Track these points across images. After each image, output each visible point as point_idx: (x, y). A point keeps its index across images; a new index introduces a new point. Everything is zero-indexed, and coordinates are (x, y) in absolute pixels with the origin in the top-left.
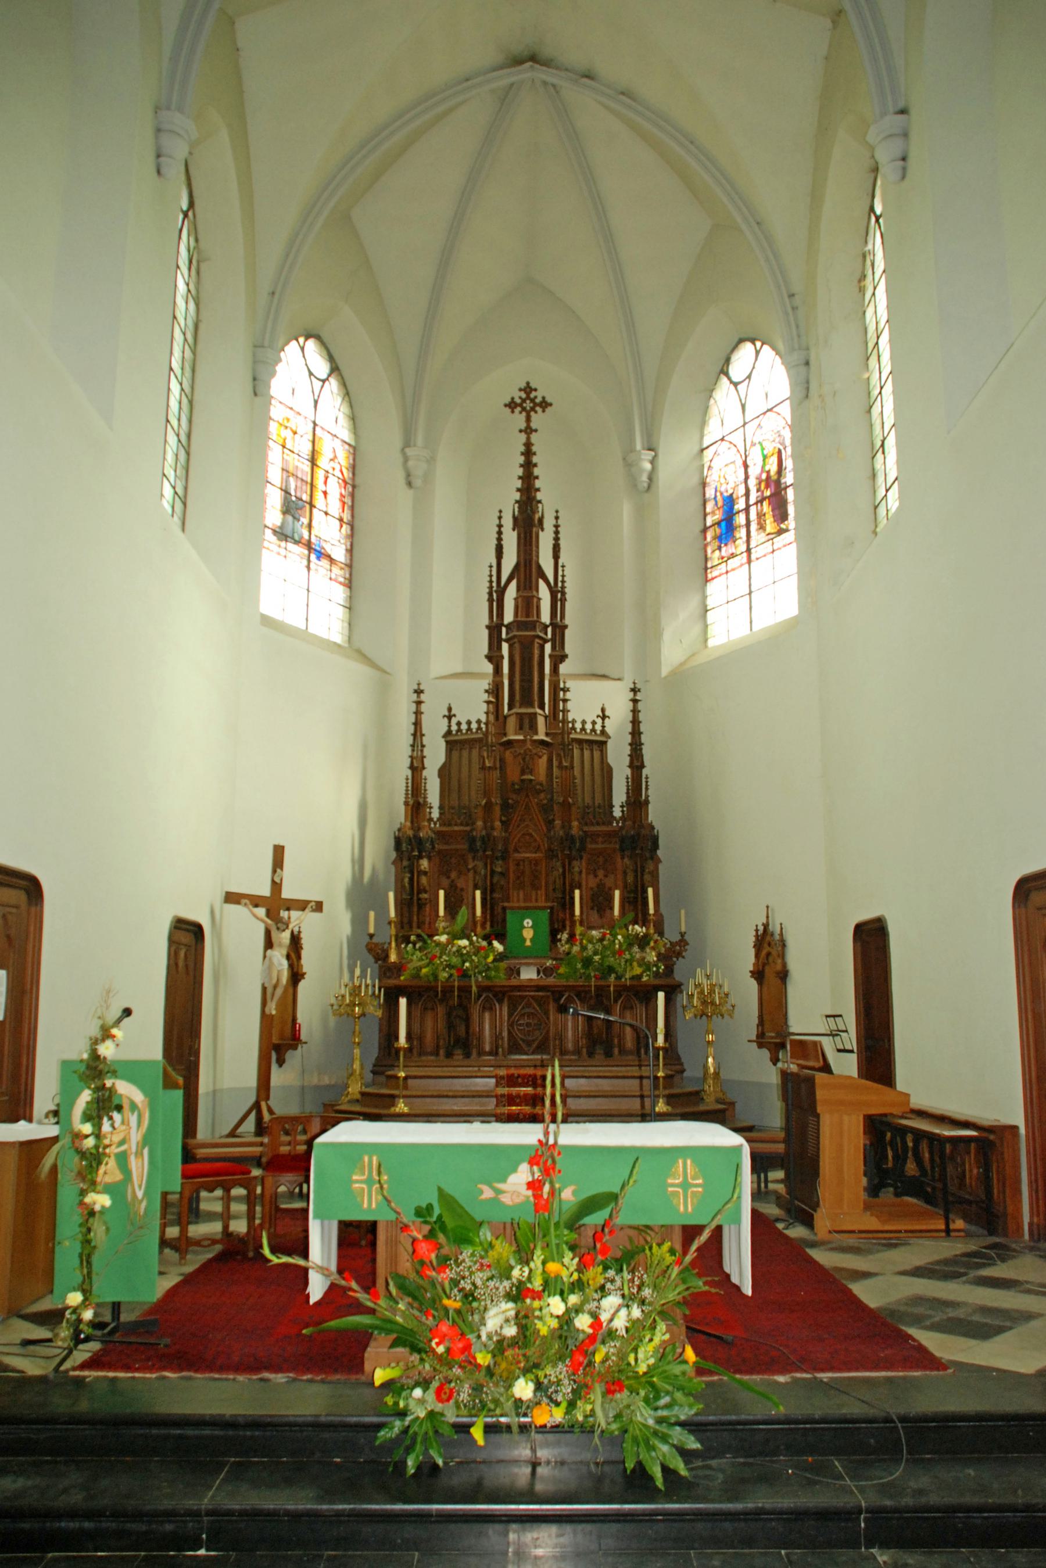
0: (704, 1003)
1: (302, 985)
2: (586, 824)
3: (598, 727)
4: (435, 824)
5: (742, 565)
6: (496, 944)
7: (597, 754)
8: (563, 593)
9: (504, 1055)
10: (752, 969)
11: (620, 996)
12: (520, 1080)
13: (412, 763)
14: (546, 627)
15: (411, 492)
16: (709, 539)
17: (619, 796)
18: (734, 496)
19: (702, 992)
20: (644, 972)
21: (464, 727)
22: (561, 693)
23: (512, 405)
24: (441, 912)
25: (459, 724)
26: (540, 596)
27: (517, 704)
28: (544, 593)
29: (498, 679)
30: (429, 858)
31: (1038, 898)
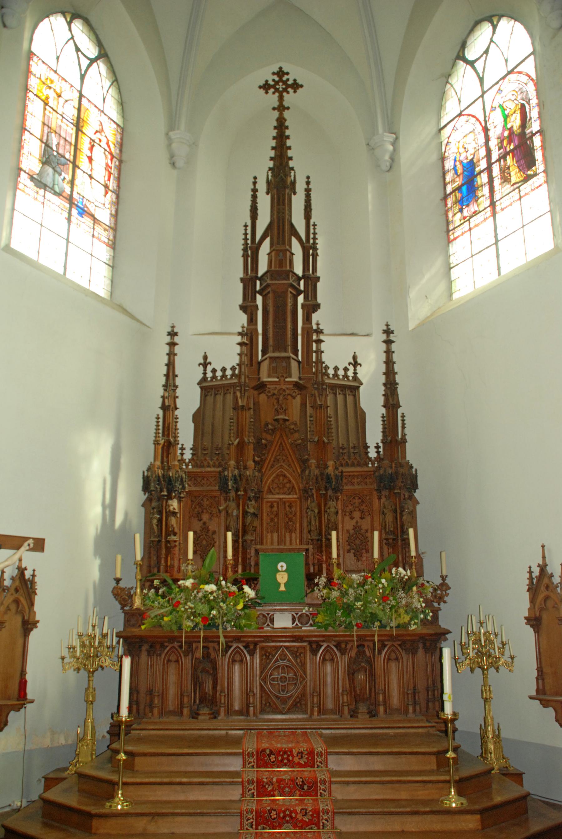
0: (480, 654)
1: (34, 636)
2: (342, 465)
3: (350, 373)
4: (187, 465)
5: (486, 219)
6: (246, 588)
7: (350, 399)
8: (315, 249)
9: (254, 714)
10: (527, 615)
11: (384, 646)
12: (273, 758)
13: (164, 402)
14: (299, 279)
15: (175, 172)
16: (449, 205)
17: (374, 435)
18: (475, 160)
19: (477, 641)
20: (412, 619)
21: (219, 374)
22: (314, 345)
23: (266, 87)
24: (190, 556)
25: (214, 371)
26: (293, 251)
27: (271, 349)
28: (296, 248)
29: (253, 327)
30: (180, 500)
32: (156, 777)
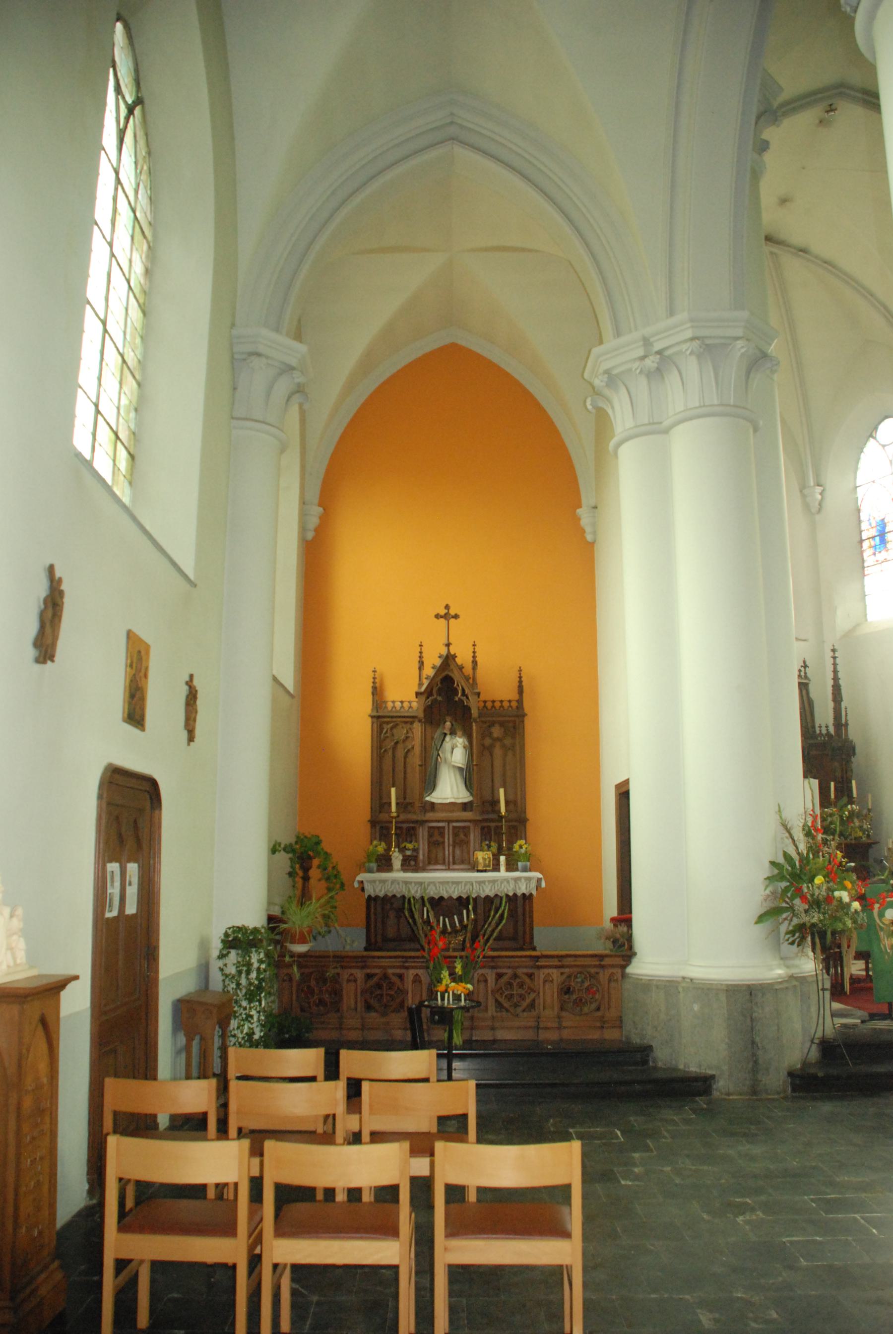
31: (146, 786)
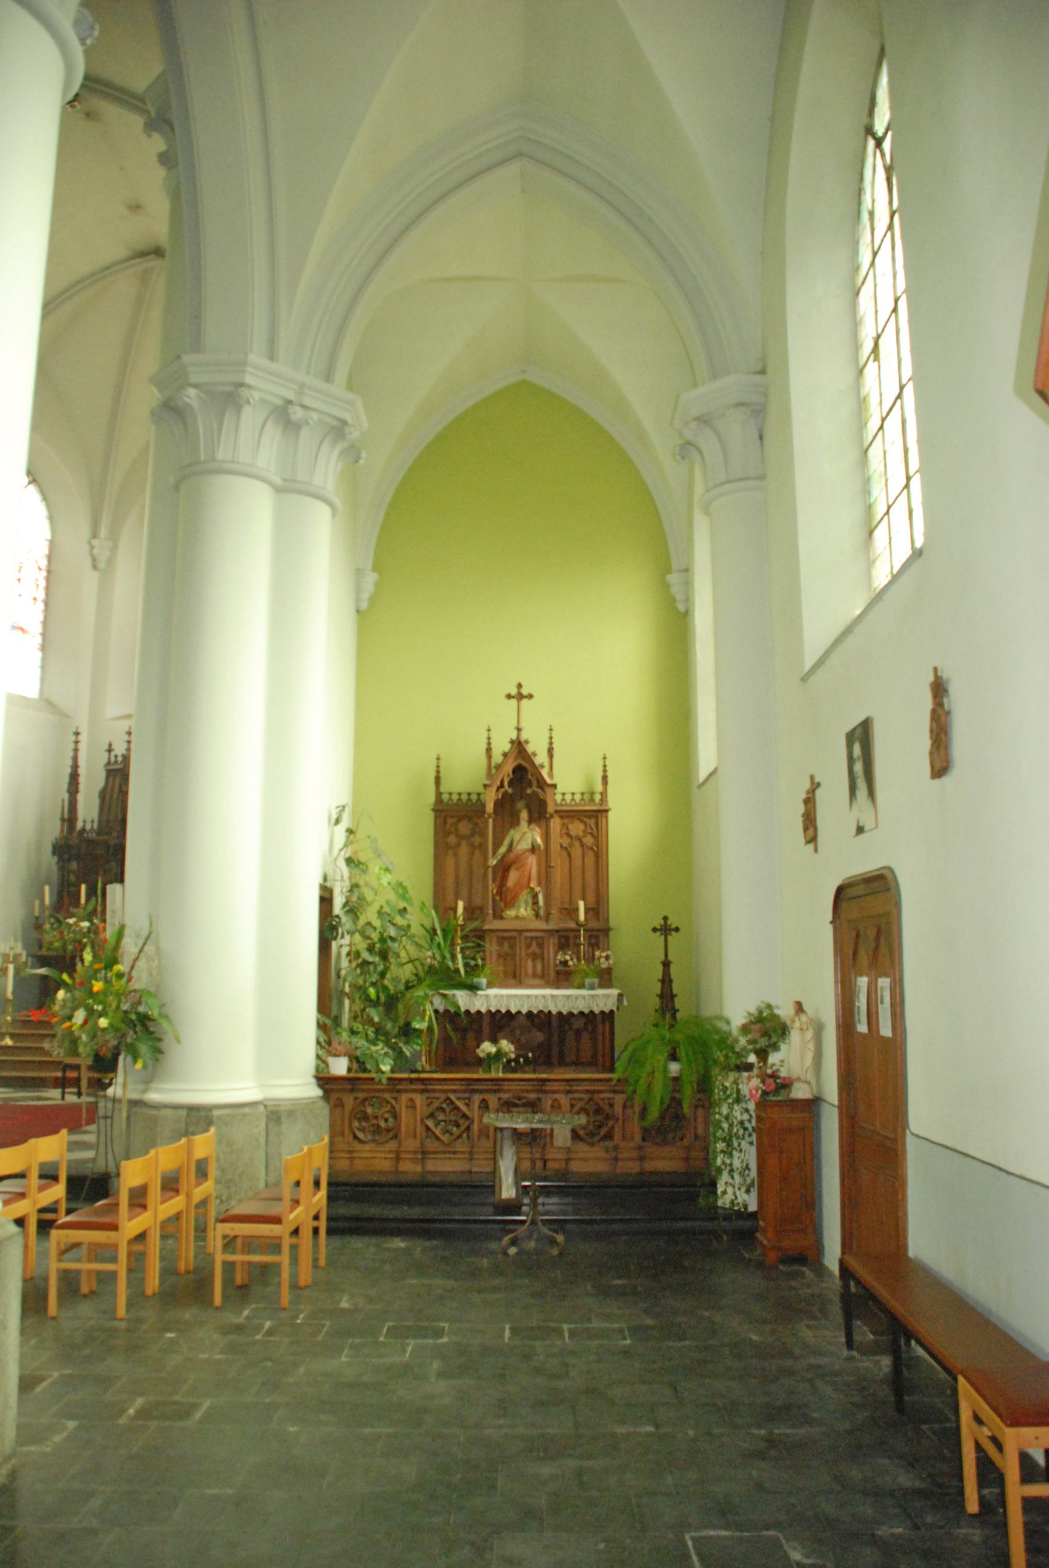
25: (116, 756)
32: (12, 1055)
